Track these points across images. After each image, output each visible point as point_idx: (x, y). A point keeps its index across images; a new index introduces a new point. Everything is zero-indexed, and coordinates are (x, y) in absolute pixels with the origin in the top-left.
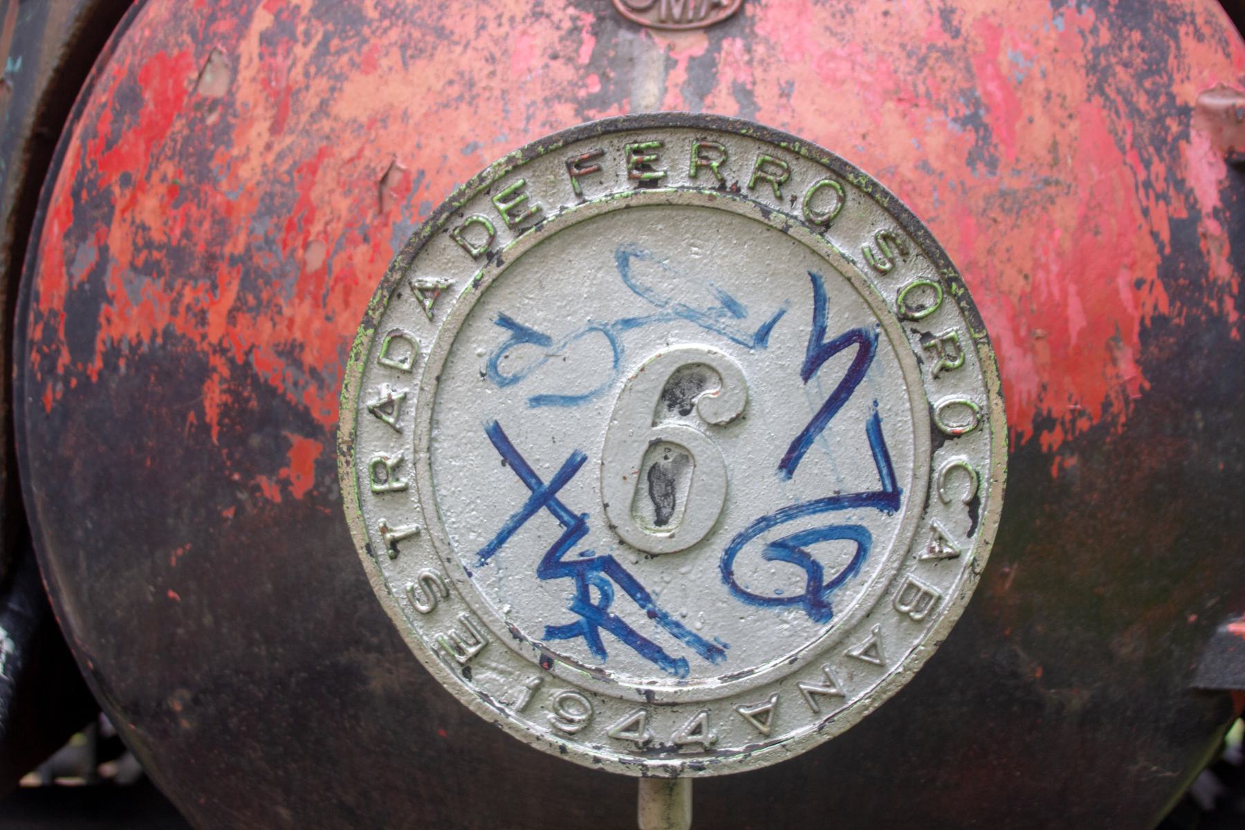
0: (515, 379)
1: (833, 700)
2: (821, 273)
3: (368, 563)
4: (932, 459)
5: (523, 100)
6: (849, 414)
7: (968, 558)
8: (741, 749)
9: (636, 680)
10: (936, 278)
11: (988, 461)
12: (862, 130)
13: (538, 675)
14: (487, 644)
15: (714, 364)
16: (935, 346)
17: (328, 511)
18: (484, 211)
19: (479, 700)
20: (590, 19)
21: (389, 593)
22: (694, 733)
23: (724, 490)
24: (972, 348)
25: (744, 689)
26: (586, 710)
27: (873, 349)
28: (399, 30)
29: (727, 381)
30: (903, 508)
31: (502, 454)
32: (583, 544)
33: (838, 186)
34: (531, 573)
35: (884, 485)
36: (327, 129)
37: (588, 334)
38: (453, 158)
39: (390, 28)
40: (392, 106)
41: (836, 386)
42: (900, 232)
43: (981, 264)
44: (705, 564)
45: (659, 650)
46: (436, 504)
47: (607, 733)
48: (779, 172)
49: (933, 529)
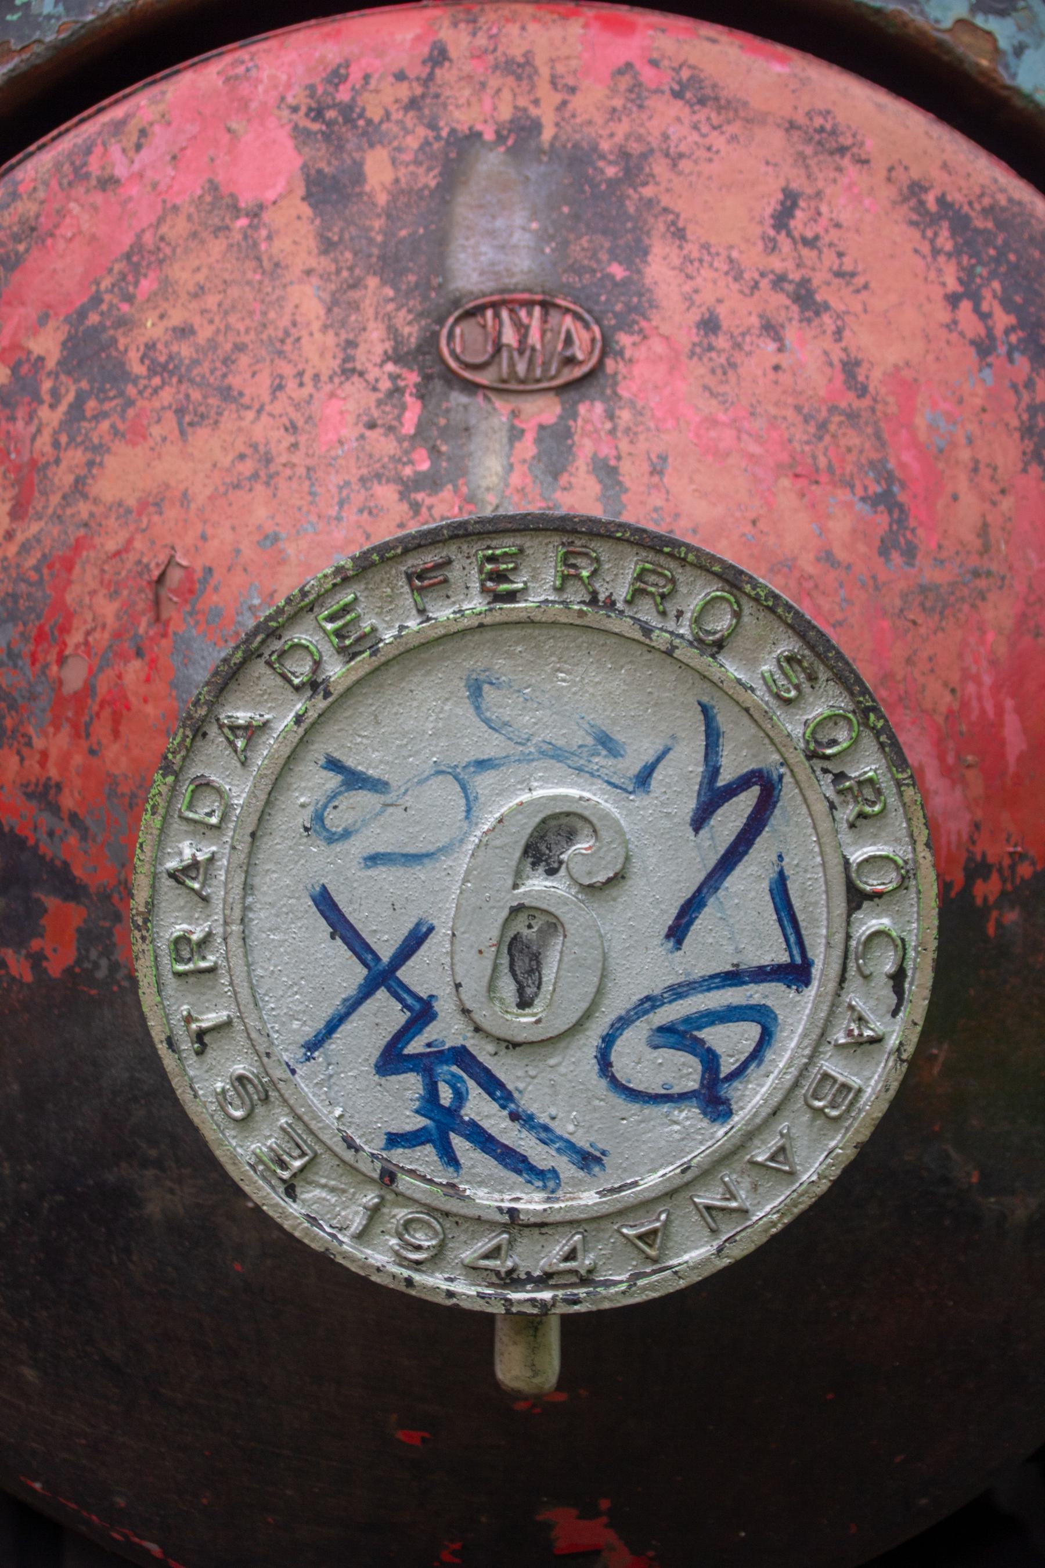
0: (346, 834)
1: (734, 1215)
2: (713, 703)
3: (169, 1061)
4: (849, 923)
5: (334, 480)
6: (749, 872)
7: (893, 1041)
8: (624, 1277)
9: (497, 1196)
10: (851, 708)
11: (915, 925)
12: (752, 515)
13: (377, 1192)
14: (316, 1155)
15: (586, 813)
16: (850, 789)
17: (94, 992)
18: (306, 632)
19: (306, 1224)
20: (413, 378)
21: (196, 1096)
22: (567, 1258)
23: (600, 965)
24: (895, 790)
25: (629, 1204)
26: (436, 1233)
27: (776, 792)
28: (174, 390)
29: (602, 833)
30: (815, 983)
31: (331, 925)
32: (431, 1033)
33: (732, 599)
34: (368, 1068)
35: (791, 956)
36: (85, 515)
37: (434, 779)
38: (248, 551)
39: (162, 387)
40: (167, 486)
41: (733, 838)
42: (807, 652)
43: (899, 678)
44: (579, 1054)
45: (524, 1159)
46: (252, 988)
47: (462, 1262)
48: (662, 582)
49: (851, 1008)
